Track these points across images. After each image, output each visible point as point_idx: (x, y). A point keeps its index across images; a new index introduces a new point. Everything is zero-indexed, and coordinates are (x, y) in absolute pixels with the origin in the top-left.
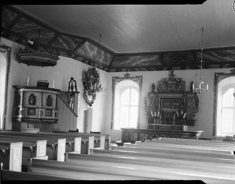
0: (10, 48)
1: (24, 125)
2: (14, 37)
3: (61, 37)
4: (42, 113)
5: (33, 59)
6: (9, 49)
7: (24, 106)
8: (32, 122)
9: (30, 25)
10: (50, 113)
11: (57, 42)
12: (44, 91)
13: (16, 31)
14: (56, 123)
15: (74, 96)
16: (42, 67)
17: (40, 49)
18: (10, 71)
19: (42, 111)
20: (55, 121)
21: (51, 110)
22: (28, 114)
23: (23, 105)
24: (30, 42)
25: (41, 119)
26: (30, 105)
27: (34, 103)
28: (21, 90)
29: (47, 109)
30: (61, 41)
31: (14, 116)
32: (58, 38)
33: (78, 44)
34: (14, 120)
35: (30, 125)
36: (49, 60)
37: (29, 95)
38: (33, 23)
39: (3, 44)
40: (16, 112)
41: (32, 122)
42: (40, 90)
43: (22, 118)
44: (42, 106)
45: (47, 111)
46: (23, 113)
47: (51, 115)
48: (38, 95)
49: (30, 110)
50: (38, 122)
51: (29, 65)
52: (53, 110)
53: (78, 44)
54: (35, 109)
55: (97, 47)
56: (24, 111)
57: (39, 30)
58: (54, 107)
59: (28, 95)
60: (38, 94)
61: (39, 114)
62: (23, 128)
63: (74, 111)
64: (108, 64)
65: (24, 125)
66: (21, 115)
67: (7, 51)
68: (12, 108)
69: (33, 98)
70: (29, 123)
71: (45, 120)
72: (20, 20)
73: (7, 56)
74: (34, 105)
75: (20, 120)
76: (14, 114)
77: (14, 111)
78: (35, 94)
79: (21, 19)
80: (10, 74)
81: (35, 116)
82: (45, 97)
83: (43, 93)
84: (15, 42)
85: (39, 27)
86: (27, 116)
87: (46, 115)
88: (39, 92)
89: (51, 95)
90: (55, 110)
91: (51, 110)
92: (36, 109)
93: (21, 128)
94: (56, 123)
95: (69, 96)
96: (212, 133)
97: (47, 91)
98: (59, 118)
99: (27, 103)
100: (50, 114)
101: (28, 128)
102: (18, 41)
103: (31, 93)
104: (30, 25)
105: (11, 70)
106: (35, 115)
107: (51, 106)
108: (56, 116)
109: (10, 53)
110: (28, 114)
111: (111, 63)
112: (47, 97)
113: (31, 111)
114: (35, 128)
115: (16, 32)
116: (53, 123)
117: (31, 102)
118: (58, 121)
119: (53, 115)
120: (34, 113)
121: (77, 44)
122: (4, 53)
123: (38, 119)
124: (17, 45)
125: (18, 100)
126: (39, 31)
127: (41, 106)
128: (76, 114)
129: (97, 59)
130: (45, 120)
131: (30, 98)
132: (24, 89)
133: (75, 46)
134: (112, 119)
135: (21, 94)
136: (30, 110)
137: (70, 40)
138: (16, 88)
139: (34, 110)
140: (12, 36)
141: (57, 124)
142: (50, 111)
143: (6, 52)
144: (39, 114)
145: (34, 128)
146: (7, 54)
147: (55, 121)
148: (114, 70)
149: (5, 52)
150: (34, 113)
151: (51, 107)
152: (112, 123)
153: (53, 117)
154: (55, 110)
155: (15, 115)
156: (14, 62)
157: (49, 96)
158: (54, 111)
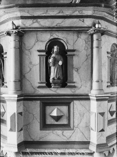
22: (45, 126)
26: (49, 85)
27: (64, 81)
49: (49, 109)
78: (69, 41)
110: (45, 126)
131: (47, 58)
139: (64, 109)
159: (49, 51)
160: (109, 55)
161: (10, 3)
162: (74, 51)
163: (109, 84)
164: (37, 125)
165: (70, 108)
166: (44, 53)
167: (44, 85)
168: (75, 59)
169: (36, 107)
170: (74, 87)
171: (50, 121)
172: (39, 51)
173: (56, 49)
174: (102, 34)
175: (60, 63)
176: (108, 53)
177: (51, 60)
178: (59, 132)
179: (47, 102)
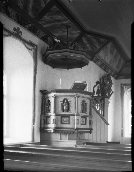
0: (36, 46)
1: (56, 137)
2: (41, 33)
3: (86, 36)
4: (78, 122)
5: (66, 56)
6: (35, 47)
7: (57, 115)
8: (63, 132)
9: (60, 17)
10: (84, 122)
11: (81, 42)
12: (79, 94)
13: (45, 24)
14: (90, 132)
15: (104, 101)
16: (68, 70)
17: (75, 44)
18: (37, 73)
19: (78, 119)
20: (89, 130)
21: (85, 117)
22: (62, 123)
23: (55, 112)
24: (56, 40)
25: (77, 129)
26: (63, 112)
27: (68, 110)
28: (52, 95)
29: (82, 117)
30: (85, 41)
31: (42, 126)
32: (83, 38)
33: (102, 45)
34: (43, 130)
35: (63, 137)
36: (82, 59)
37: (62, 100)
38: (63, 15)
39: (29, 40)
40: (44, 121)
41: (66, 133)
42: (75, 94)
43: (55, 128)
44: (78, 112)
45: (82, 119)
46: (55, 121)
47: (86, 124)
48: (72, 100)
49: (63, 118)
50: (74, 132)
51: (54, 68)
52: (87, 118)
53: (102, 45)
54: (69, 116)
55: (117, 50)
56: (56, 119)
57: (67, 26)
58: (88, 114)
59: (60, 100)
60: (73, 98)
61: (75, 123)
62: (55, 140)
63: (105, 118)
64: (118, 71)
65: (56, 137)
66: (54, 124)
67: (34, 49)
68: (40, 116)
69: (66, 103)
70: (62, 134)
71: (81, 130)
72: (51, 9)
73: (33, 55)
74: (68, 112)
75: (52, 131)
76: (42, 123)
77: (43, 121)
78: (69, 99)
79: (53, 8)
80: (37, 75)
81: (69, 125)
82: (80, 100)
83: (78, 97)
84: (41, 39)
85: (68, 22)
86: (60, 125)
87: (81, 124)
88: (74, 96)
89: (85, 99)
90: (90, 117)
91: (85, 117)
92: (71, 116)
93: (52, 140)
94: (90, 132)
95: (99, 100)
96: (120, 134)
97: (82, 95)
98: (94, 127)
99: (59, 109)
100: (84, 123)
101: (61, 139)
102: (44, 39)
103: (64, 98)
104: (60, 17)
105: (38, 72)
106: (69, 123)
107: (85, 113)
108: (90, 124)
109: (37, 52)
110: (62, 123)
111: (121, 70)
112: (82, 102)
113: (65, 119)
114: (70, 140)
115: (44, 26)
116: (83, 133)
117: (65, 108)
118: (92, 130)
119: (88, 123)
120: (68, 122)
121: (100, 45)
122: (30, 51)
123: (73, 128)
124: (43, 43)
125: (47, 107)
126: (68, 27)
127: (77, 113)
128: (106, 120)
129: (111, 65)
130: (81, 130)
131: (63, 104)
132: (55, 94)
133: (98, 47)
134: (122, 127)
135: (52, 100)
136: (61, 118)
137: (94, 40)
138: (44, 93)
139: (68, 118)
140: (39, 31)
141: (92, 134)
142: (84, 119)
143: (33, 50)
144: (75, 123)
145: (69, 140)
146: (34, 53)
147: (89, 130)
148: (123, 76)
149: (31, 50)
150: (68, 122)
151: (85, 114)
152: (122, 130)
153: (88, 126)
154: (89, 118)
155: (44, 124)
156: (40, 63)
157: (84, 101)
158: (88, 119)
159: (64, 102)
160: (82, 103)
161: (101, 100)
162: (71, 102)
163: (82, 112)
164: (60, 123)
165: (53, 170)
166: (62, 102)
167: (69, 102)
168: (71, 104)
169: (59, 117)
170: (70, 112)
171: (63, 122)
172: (61, 102)
173: (65, 101)
174: (78, 97)
175: (67, 105)
176: (81, 102)
177: (64, 104)
178: (66, 125)
179: (62, 116)
